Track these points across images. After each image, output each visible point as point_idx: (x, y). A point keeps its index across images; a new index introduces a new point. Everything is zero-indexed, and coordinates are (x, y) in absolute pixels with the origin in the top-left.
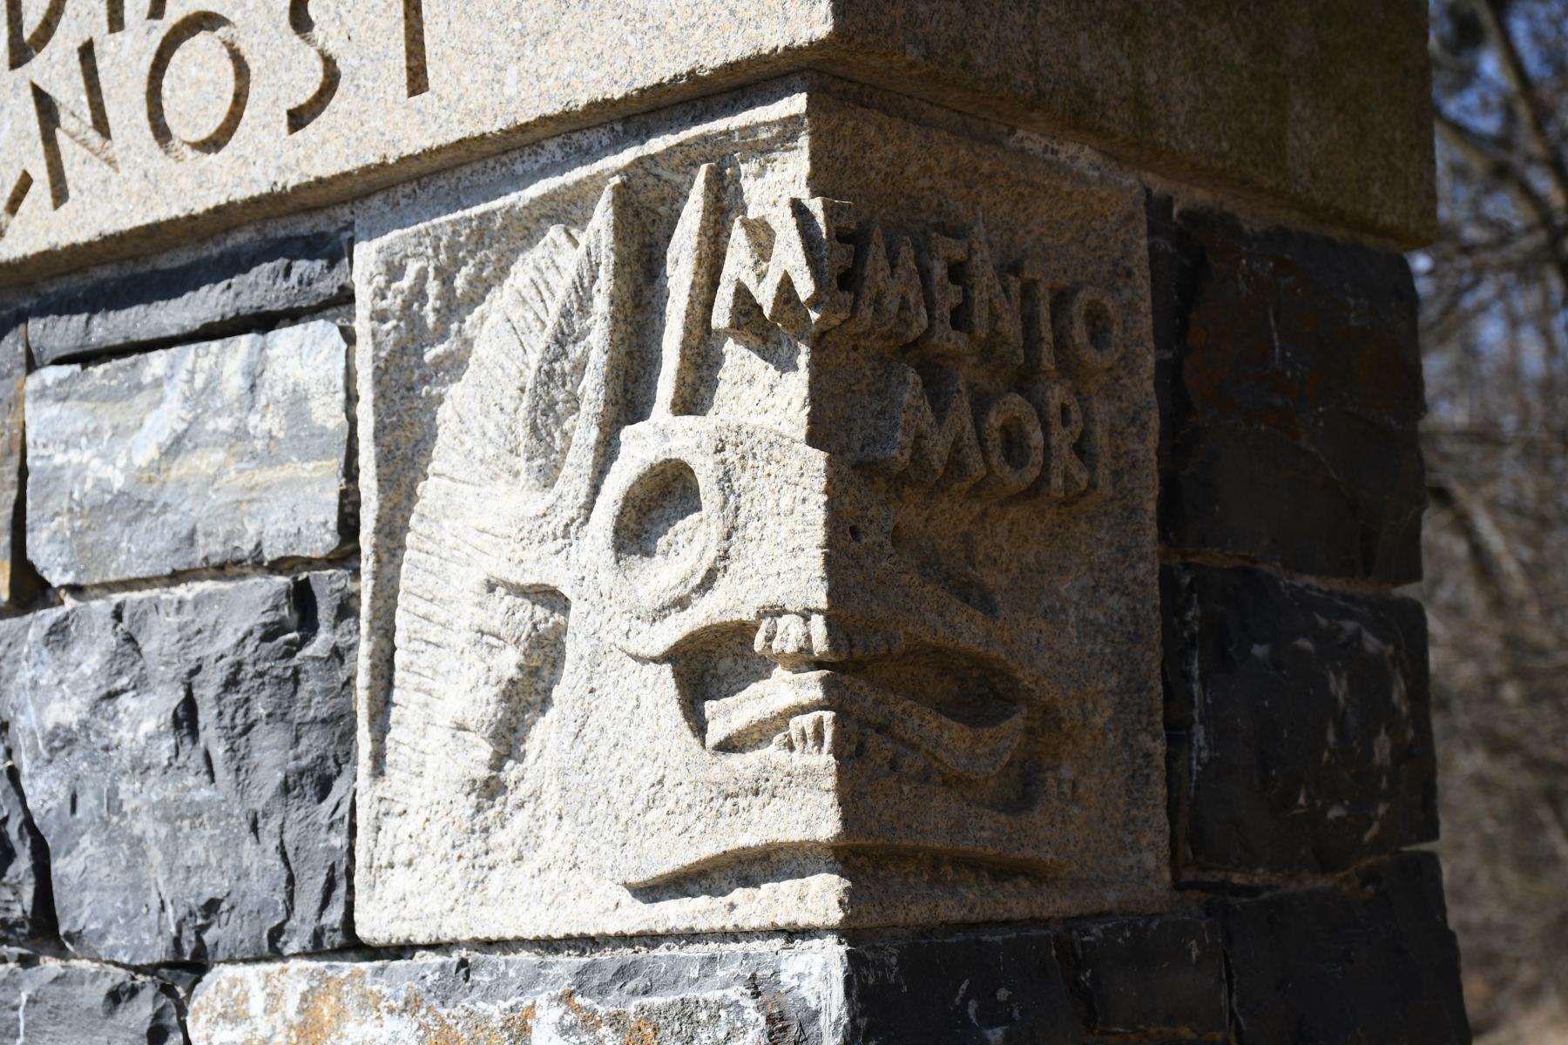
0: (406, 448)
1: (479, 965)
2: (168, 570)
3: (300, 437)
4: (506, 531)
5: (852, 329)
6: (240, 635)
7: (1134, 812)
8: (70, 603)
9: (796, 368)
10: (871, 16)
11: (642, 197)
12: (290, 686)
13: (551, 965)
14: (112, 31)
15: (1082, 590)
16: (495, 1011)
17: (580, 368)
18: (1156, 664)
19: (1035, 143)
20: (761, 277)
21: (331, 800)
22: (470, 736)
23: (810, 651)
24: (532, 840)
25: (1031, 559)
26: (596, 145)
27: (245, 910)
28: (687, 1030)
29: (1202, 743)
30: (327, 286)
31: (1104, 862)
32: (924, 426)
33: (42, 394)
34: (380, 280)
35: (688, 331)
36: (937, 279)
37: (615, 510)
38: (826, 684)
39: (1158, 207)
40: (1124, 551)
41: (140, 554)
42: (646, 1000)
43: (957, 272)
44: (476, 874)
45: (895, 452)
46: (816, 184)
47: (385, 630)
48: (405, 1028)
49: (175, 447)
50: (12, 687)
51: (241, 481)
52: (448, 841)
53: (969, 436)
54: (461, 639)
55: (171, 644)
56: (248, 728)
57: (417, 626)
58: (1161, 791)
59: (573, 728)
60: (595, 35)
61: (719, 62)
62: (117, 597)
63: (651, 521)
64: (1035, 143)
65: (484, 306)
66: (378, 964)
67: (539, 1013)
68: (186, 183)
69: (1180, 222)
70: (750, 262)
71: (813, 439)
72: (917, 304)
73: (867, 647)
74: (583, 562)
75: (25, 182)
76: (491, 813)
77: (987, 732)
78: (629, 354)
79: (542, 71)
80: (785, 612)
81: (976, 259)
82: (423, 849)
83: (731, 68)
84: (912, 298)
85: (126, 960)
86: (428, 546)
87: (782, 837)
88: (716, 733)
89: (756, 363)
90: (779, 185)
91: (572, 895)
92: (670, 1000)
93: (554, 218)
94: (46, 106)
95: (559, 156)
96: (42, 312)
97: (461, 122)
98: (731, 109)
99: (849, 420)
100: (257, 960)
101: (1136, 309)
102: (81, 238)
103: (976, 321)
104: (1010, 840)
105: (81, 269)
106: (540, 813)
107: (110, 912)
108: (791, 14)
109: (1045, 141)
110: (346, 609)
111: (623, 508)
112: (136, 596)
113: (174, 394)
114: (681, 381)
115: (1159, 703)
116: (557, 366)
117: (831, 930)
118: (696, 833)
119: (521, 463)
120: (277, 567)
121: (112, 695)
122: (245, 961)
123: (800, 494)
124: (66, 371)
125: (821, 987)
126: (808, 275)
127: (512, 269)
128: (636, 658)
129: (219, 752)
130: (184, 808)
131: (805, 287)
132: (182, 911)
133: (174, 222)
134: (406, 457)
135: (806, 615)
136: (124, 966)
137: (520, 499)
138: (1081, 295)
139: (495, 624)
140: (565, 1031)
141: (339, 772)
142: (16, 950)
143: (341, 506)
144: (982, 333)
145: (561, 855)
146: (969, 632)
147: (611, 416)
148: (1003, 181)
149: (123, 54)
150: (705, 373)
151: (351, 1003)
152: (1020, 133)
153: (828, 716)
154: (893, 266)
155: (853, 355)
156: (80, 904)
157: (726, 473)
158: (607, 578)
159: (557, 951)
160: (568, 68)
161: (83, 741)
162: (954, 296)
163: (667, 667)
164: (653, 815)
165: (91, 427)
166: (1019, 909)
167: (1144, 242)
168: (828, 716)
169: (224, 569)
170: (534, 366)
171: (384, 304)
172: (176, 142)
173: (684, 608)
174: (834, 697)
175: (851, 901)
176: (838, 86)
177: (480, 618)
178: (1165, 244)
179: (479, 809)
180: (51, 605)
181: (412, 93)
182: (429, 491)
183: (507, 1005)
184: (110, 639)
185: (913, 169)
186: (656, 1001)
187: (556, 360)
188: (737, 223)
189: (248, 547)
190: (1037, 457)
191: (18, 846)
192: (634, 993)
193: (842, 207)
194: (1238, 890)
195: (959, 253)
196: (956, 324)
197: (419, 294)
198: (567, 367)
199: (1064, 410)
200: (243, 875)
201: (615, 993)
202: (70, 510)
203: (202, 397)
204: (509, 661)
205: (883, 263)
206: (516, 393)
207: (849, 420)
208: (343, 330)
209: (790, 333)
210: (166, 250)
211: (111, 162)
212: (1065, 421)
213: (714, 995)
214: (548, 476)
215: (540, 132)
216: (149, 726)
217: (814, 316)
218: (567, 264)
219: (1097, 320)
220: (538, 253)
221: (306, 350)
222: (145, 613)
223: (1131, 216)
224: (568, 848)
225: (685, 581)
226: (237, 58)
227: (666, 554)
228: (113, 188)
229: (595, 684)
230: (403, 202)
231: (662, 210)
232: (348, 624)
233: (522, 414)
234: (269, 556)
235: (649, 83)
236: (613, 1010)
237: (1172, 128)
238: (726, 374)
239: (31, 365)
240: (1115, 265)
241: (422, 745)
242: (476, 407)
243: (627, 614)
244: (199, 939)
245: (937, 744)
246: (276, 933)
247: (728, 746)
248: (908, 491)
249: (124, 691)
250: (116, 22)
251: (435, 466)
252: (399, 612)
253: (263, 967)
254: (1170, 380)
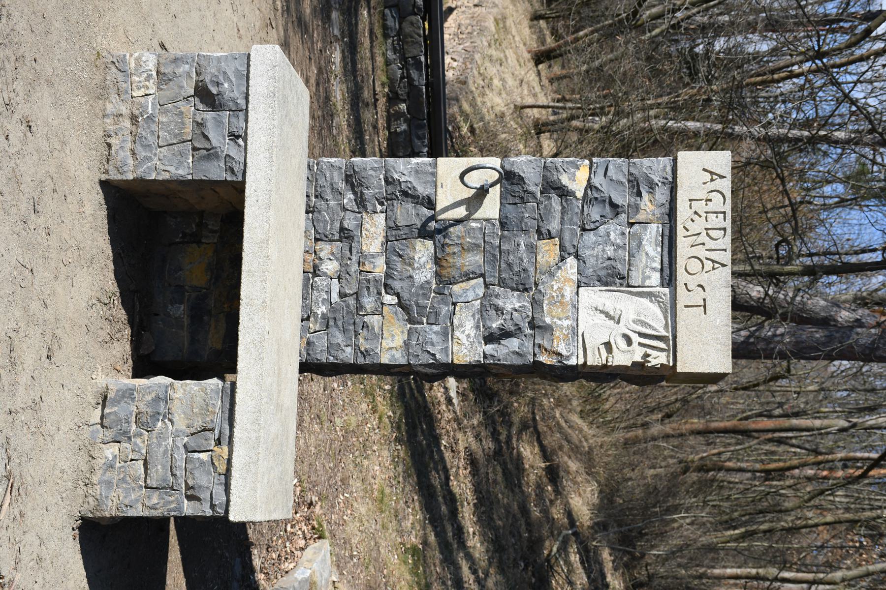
75: (687, 230)
110: (621, 285)
131: (649, 365)
204: (612, 313)
214: (634, 322)
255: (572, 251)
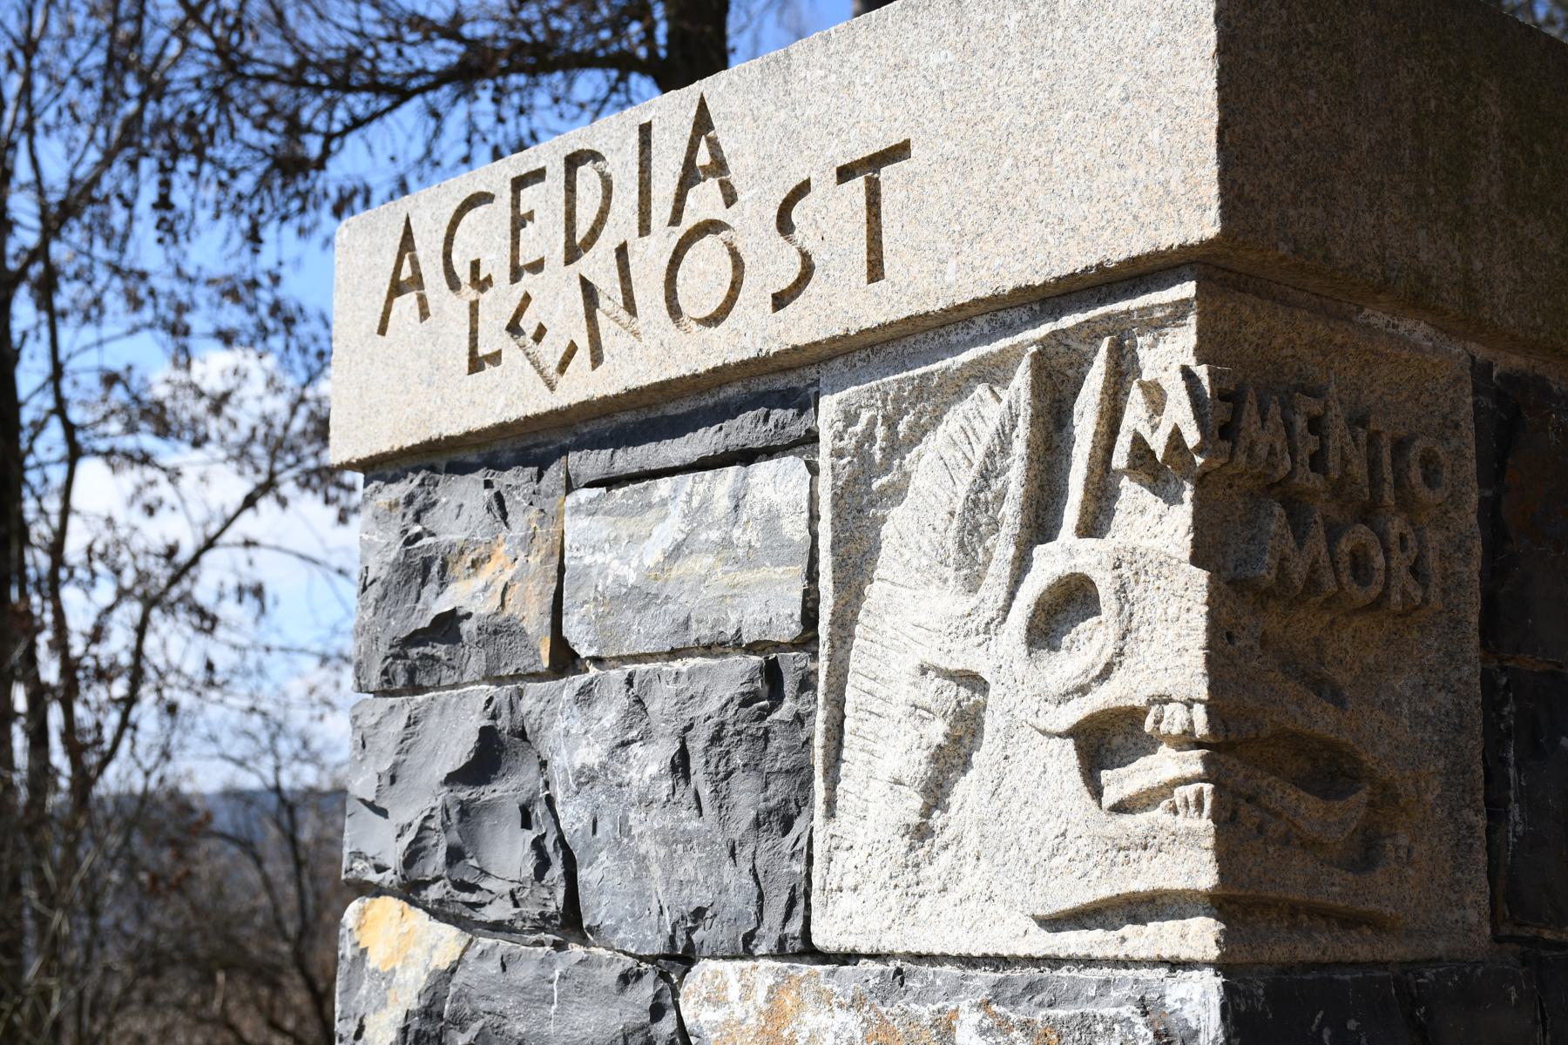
0: (856, 558)
1: (911, 974)
2: (668, 648)
3: (774, 547)
4: (938, 626)
5: (1229, 471)
6: (723, 701)
7: (1459, 875)
8: (593, 671)
9: (1182, 502)
10: (1251, 220)
11: (1054, 363)
12: (761, 743)
13: (972, 978)
14: (641, 235)
15: (1414, 687)
16: (925, 1012)
17: (1000, 497)
18: (1479, 750)
19: (1380, 320)
20: (1155, 428)
21: (792, 836)
22: (904, 790)
23: (1192, 733)
24: (954, 876)
25: (1371, 660)
26: (1018, 322)
27: (725, 918)
28: (1086, 1039)
29: (1517, 818)
30: (797, 429)
31: (1433, 916)
32: (1287, 551)
33: (577, 510)
34: (840, 425)
35: (1091, 470)
36: (1298, 430)
37: (1029, 612)
38: (1206, 761)
39: (1481, 371)
40: (1451, 656)
41: (647, 635)
42: (1051, 1012)
43: (1315, 424)
44: (909, 901)
45: (1263, 572)
46: (1201, 354)
47: (837, 702)
48: (851, 1022)
49: (676, 552)
50: (550, 734)
51: (726, 580)
52: (886, 873)
53: (1324, 559)
54: (898, 711)
55: (670, 707)
56: (728, 775)
57: (863, 699)
58: (1482, 858)
59: (990, 787)
60: (1020, 236)
61: (1123, 257)
62: (630, 668)
63: (1057, 622)
64: (1380, 320)
65: (921, 446)
66: (829, 967)
67: (961, 1016)
68: (692, 350)
69: (1498, 383)
70: (1146, 416)
71: (1196, 560)
72: (1282, 451)
73: (1240, 732)
74: (1000, 653)
75: (572, 350)
76: (921, 852)
77: (1338, 804)
78: (1041, 487)
79: (977, 263)
80: (1172, 700)
81: (1331, 414)
82: (866, 878)
83: (1133, 261)
84: (1278, 447)
85: (633, 951)
86: (872, 636)
87: (1167, 886)
88: (1111, 796)
89: (1147, 497)
90: (1170, 356)
91: (988, 922)
92: (1071, 1013)
93: (980, 378)
94: (589, 292)
95: (986, 329)
96: (578, 447)
97: (909, 303)
98: (1130, 293)
99: (1225, 544)
100: (733, 958)
101: (1462, 456)
102: (611, 392)
103: (1331, 464)
104: (1356, 895)
105: (609, 415)
106: (961, 853)
107: (621, 912)
108: (1185, 219)
109: (1387, 318)
110: (806, 684)
111: (1035, 611)
112: (643, 667)
113: (676, 510)
114: (1084, 511)
115: (1481, 784)
116: (981, 495)
117: (1208, 964)
118: (1093, 878)
119: (949, 572)
120: (752, 648)
121: (625, 744)
122: (724, 958)
123: (1185, 604)
124: (595, 492)
125: (1200, 1011)
126: (1195, 427)
127: (945, 418)
128: (1044, 732)
129: (706, 792)
130: (678, 835)
131: (1192, 437)
132: (676, 916)
133: (681, 380)
134: (856, 565)
135: (1189, 704)
136: (630, 955)
137: (949, 602)
138: (1417, 443)
139: (927, 700)
140: (983, 1032)
141: (799, 813)
142: (551, 937)
143: (804, 602)
144: (1334, 475)
145: (978, 889)
146: (1323, 721)
147: (1024, 537)
148: (1352, 350)
149: (649, 253)
150: (1104, 504)
151: (809, 999)
152: (1367, 311)
153: (1208, 788)
154: (1263, 420)
155: (1229, 491)
156: (599, 904)
157: (1122, 586)
158: (1020, 667)
159: (975, 967)
160: (998, 261)
161: (602, 778)
162: (1312, 444)
163: (1070, 743)
164: (1056, 861)
165: (613, 535)
166: (1363, 953)
167: (1470, 400)
168: (1208, 788)
169: (711, 649)
170: (963, 495)
171: (842, 444)
172: (685, 319)
173: (1085, 694)
174: (1212, 772)
175: (1227, 940)
176: (1219, 275)
177: (915, 695)
178: (1486, 401)
179: (911, 848)
180: (578, 672)
181: (871, 281)
182: (875, 593)
183: (935, 1008)
184: (624, 701)
185: (1279, 341)
186: (1060, 1013)
187: (981, 491)
188: (1135, 384)
189: (731, 632)
190: (1380, 577)
191: (553, 857)
192: (1040, 1005)
193: (1223, 373)
194: (1548, 945)
195: (1316, 408)
196: (1313, 468)
197: (869, 436)
198: (990, 496)
199: (1402, 538)
200: (723, 890)
201: (1025, 1004)
202: (595, 599)
203: (697, 514)
204: (937, 731)
205: (1256, 417)
206: (947, 516)
207: (1225, 544)
208: (808, 464)
209: (1178, 474)
210: (673, 400)
211: (636, 334)
212: (1403, 548)
213: (1109, 1012)
214: (973, 584)
215: (972, 311)
216: (653, 769)
217: (1199, 460)
218: (993, 414)
219: (1430, 464)
220: (967, 405)
221: (778, 479)
222: (650, 681)
223: (1458, 379)
224: (983, 885)
225: (1086, 672)
226: (734, 254)
227: (1069, 649)
228: (637, 354)
229: (1008, 753)
230: (859, 364)
231: (1070, 372)
232: (807, 695)
233: (952, 533)
234: (746, 640)
235: (1064, 273)
236: (1023, 1018)
237: (1494, 307)
238: (1121, 505)
239: (569, 488)
240: (1445, 418)
241: (866, 794)
242: (913, 526)
243: (1037, 699)
244: (689, 938)
245: (1296, 813)
246: (749, 938)
247: (1120, 808)
248: (1272, 603)
249: (634, 741)
250: (644, 229)
251: (879, 572)
252: (848, 687)
253: (738, 964)
254: (1490, 513)
255: (645, 991)
